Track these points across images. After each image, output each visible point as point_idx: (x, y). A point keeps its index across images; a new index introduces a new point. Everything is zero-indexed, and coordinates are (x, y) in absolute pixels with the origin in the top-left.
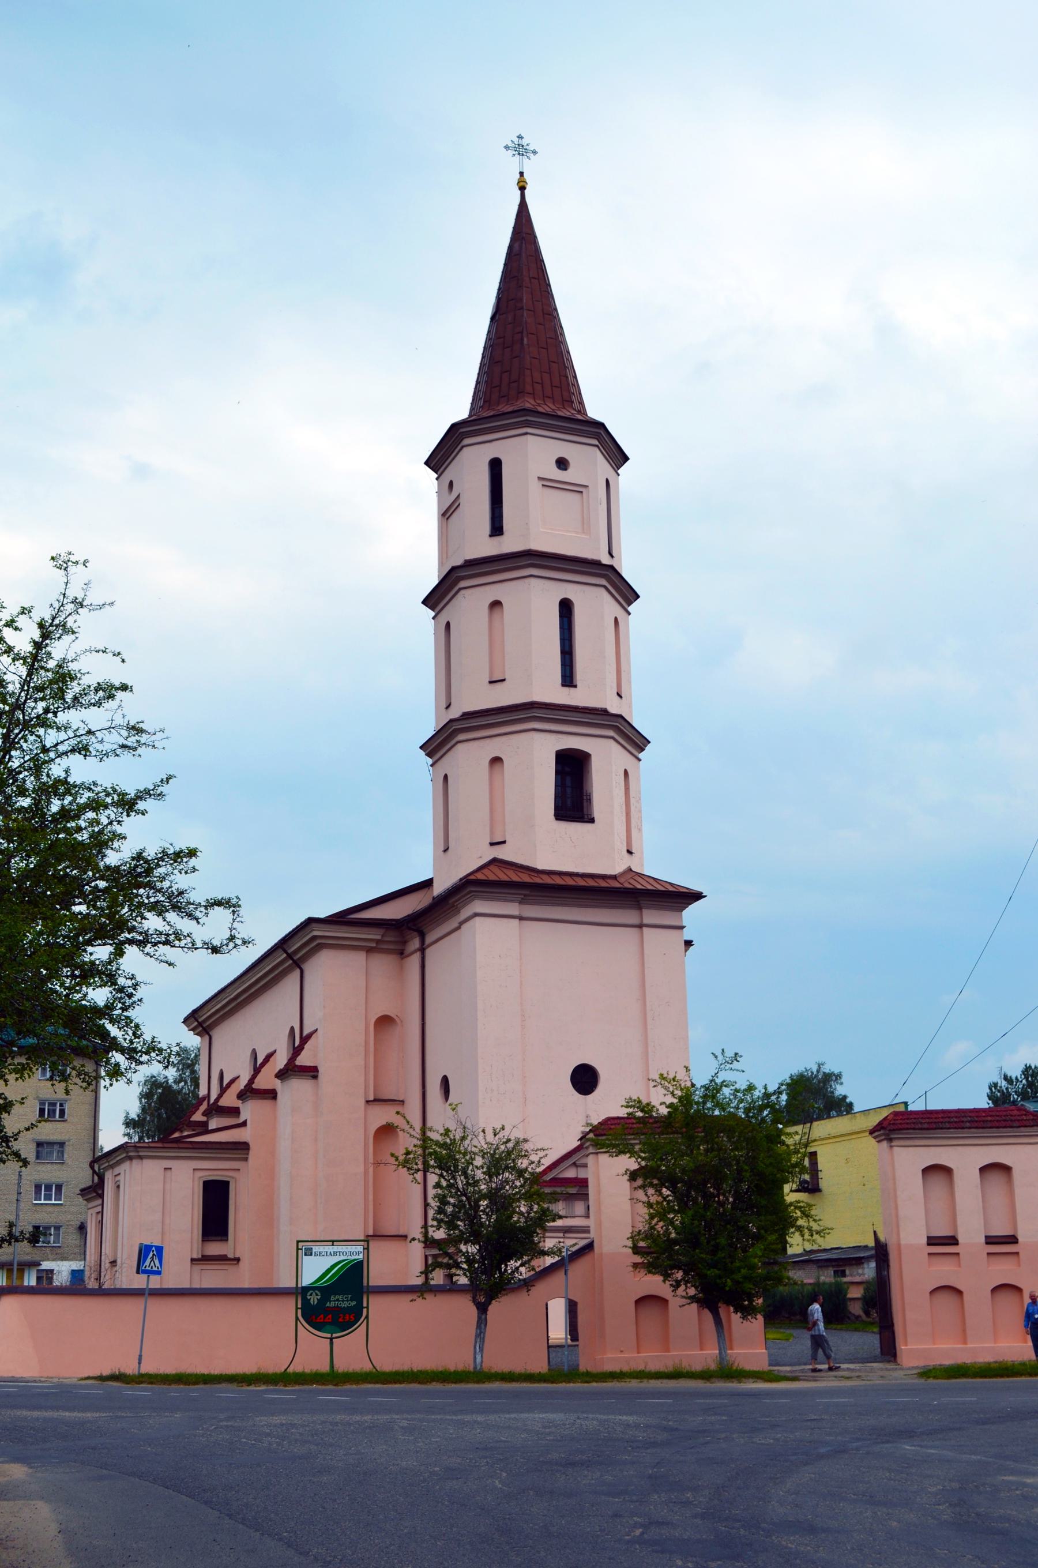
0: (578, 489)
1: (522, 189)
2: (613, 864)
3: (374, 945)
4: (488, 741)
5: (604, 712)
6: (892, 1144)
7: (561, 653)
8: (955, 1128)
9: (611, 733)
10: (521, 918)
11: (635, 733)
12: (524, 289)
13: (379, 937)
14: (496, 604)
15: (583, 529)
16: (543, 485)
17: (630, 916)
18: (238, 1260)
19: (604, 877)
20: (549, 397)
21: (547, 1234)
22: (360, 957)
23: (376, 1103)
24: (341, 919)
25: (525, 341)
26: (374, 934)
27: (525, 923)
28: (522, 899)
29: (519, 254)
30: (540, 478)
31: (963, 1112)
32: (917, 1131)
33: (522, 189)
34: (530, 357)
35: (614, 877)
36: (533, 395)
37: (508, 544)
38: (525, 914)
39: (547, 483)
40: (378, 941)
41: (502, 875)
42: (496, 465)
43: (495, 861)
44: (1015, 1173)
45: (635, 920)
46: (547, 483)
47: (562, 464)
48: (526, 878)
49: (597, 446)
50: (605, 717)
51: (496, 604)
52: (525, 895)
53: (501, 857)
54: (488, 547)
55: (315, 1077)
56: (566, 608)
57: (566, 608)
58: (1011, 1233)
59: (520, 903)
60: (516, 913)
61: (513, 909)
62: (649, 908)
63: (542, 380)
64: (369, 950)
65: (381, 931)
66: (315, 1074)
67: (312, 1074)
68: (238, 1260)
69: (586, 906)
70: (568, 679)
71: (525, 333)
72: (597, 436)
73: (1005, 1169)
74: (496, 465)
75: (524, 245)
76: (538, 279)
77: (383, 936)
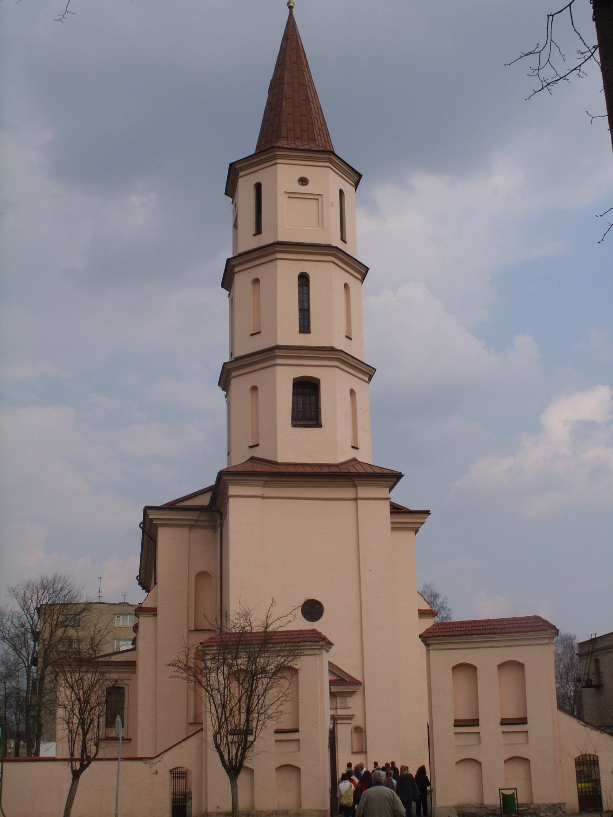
0: (315, 197)
1: (291, 8)
2: (340, 454)
3: (194, 523)
4: (249, 375)
5: (332, 349)
6: (429, 648)
7: (300, 310)
8: (478, 634)
9: (336, 363)
10: (263, 497)
11: (359, 363)
12: (286, 70)
13: (196, 518)
14: (256, 281)
15: (319, 225)
16: (289, 197)
17: (349, 493)
18: (130, 740)
19: (329, 465)
20: (299, 139)
21: (338, 722)
22: (185, 531)
23: (195, 632)
24: (171, 507)
25: (284, 104)
26: (193, 516)
27: (265, 500)
28: (264, 484)
29: (285, 49)
30: (286, 193)
31: (485, 622)
32: (447, 638)
33: (291, 8)
34: (287, 114)
35: (337, 465)
36: (287, 138)
37: (265, 239)
38: (266, 495)
39: (291, 195)
40: (196, 521)
41: (258, 468)
42: (258, 187)
43: (253, 459)
44: (527, 668)
45: (353, 496)
46: (291, 195)
47: (303, 181)
48: (266, 469)
49: (330, 167)
50: (331, 352)
51: (256, 281)
52: (266, 481)
53: (256, 455)
54: (249, 242)
55: (156, 615)
56: (304, 279)
57: (304, 279)
58: (476, 718)
59: (263, 487)
60: (260, 494)
61: (258, 491)
62: (362, 485)
63: (294, 128)
64: (191, 527)
65: (197, 513)
66: (155, 613)
67: (152, 613)
68: (130, 740)
69: (344, 487)
70: (305, 327)
71: (284, 98)
72: (330, 161)
73: (520, 666)
74: (258, 187)
75: (288, 43)
76: (297, 63)
77: (198, 517)
